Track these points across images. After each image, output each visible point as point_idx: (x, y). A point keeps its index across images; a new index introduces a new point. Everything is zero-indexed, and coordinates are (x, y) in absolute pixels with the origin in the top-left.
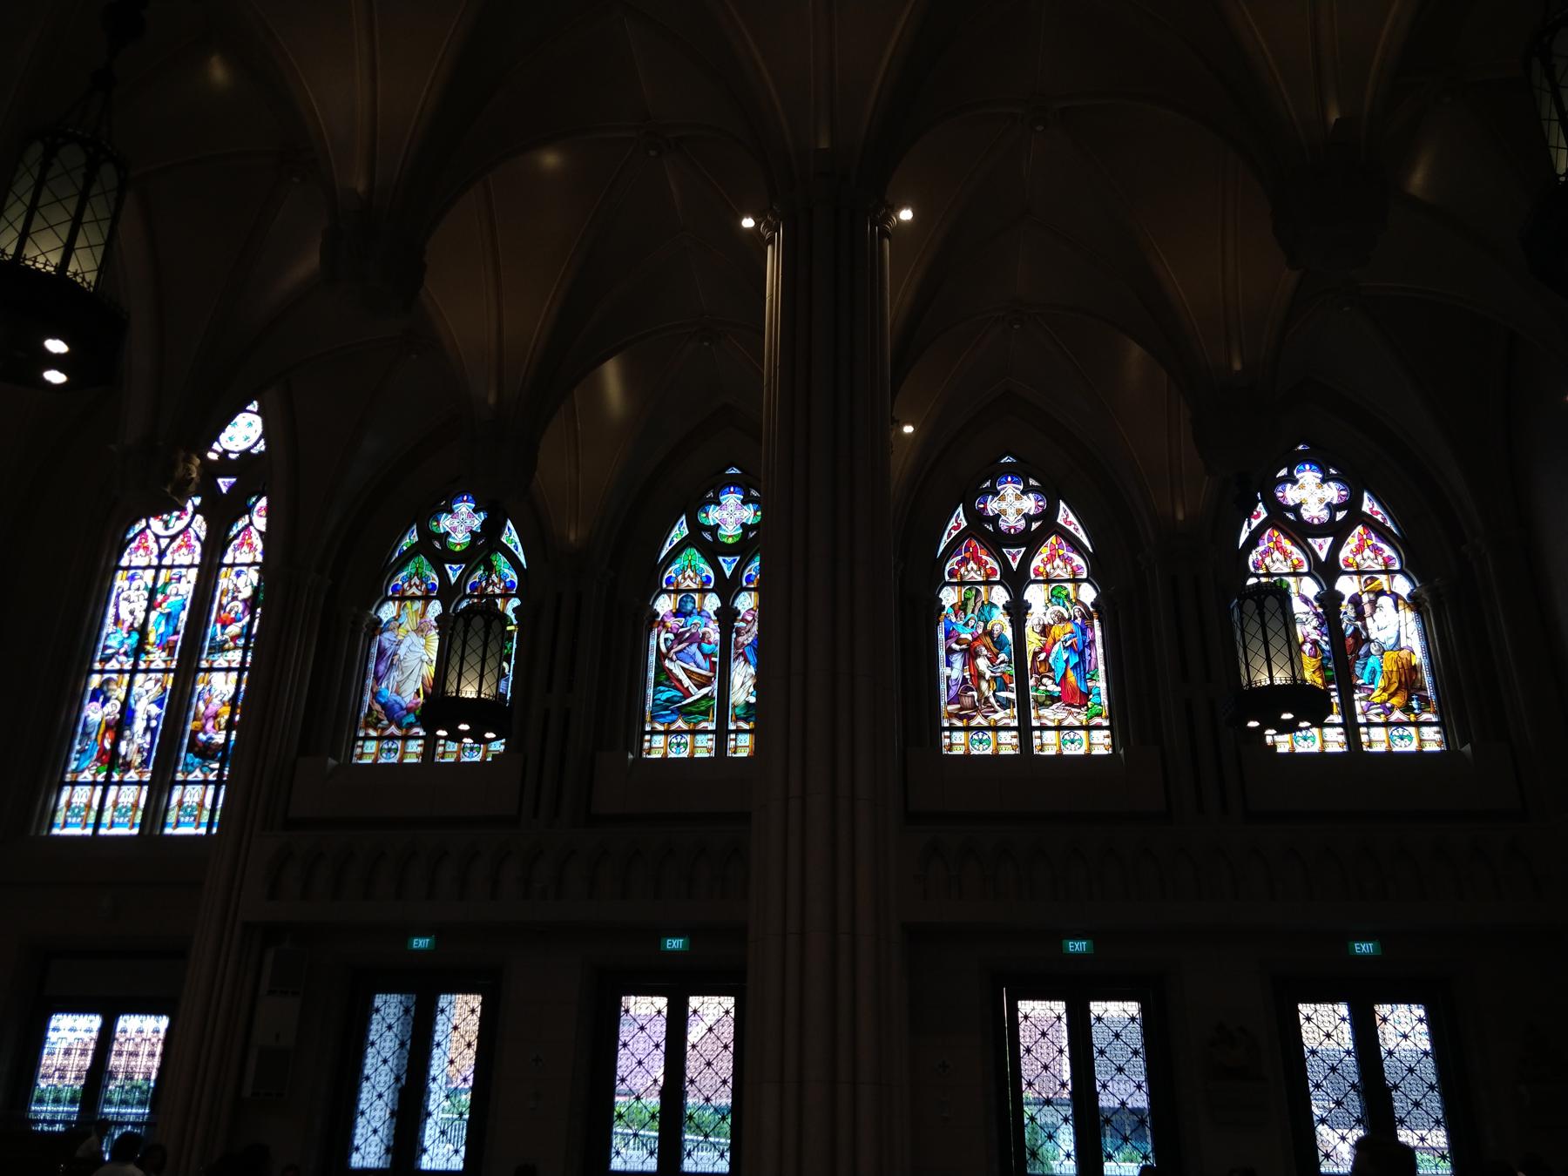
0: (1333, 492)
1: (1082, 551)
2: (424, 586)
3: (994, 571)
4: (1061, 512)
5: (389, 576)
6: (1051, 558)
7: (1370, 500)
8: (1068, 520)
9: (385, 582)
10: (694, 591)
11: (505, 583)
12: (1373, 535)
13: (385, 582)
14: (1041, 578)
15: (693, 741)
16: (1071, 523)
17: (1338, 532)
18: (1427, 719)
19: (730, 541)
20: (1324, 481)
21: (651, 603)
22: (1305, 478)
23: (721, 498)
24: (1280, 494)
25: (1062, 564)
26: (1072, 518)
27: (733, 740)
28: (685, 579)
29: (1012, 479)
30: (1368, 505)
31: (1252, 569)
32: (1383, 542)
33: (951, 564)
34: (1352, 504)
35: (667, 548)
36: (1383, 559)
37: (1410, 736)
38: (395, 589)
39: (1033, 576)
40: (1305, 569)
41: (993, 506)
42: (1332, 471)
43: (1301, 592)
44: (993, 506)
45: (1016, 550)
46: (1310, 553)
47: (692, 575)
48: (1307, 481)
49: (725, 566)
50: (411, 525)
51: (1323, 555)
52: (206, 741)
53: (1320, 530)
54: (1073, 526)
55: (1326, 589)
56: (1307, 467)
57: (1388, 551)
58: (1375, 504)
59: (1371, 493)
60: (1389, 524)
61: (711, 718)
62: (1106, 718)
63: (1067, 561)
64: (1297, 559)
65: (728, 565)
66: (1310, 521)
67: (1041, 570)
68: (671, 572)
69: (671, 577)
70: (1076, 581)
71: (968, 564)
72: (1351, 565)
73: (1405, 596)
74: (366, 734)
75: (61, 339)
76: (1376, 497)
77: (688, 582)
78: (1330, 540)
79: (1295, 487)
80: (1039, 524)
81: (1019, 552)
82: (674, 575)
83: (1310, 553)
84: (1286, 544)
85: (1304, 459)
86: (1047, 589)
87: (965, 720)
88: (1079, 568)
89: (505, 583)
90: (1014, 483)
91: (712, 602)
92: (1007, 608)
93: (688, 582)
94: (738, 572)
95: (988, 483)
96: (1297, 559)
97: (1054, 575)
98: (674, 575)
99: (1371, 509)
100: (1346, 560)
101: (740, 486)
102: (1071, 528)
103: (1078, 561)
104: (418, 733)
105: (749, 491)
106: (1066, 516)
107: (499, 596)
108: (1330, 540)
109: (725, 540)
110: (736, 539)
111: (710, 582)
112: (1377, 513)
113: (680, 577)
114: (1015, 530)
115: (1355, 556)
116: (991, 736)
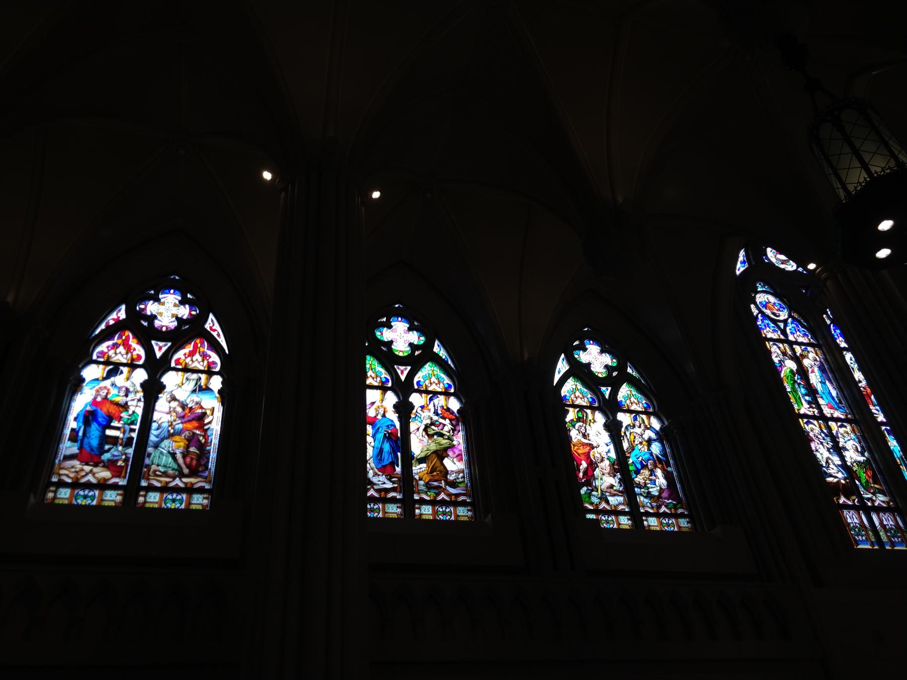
0: (415, 338)
2: (129, 355)
3: (139, 357)
4: (209, 321)
5: (171, 353)
6: (192, 354)
7: (438, 346)
8: (214, 328)
9: (170, 354)
10: (124, 365)
11: (381, 378)
12: (206, 343)
13: (170, 354)
14: (180, 367)
15: (101, 495)
16: (215, 330)
18: (622, 509)
19: (401, 354)
20: (410, 329)
21: (158, 377)
22: (397, 326)
23: (161, 296)
24: (576, 356)
25: (200, 359)
26: (217, 326)
27: (52, 491)
28: (431, 384)
29: (174, 292)
30: (438, 349)
31: (416, 387)
32: (212, 351)
33: (103, 347)
34: (621, 368)
36: (208, 362)
37: (94, 496)
38: (178, 362)
39: (173, 364)
41: (151, 308)
42: (416, 323)
43: (208, 385)
44: (151, 308)
45: (404, 367)
46: (150, 351)
47: (373, 375)
48: (167, 301)
49: (156, 348)
50: (119, 304)
52: (885, 525)
53: (403, 361)
54: (216, 333)
55: (401, 399)
56: (400, 319)
57: (447, 381)
58: (442, 349)
59: (440, 341)
60: (450, 362)
61: (123, 474)
62: (400, 492)
63: (204, 356)
64: (591, 397)
66: (159, 329)
67: (181, 361)
68: (419, 378)
69: (420, 381)
70: (210, 373)
71: (117, 348)
72: (181, 364)
73: (455, 411)
74: (149, 484)
75: (264, 178)
76: (444, 345)
77: (119, 357)
79: (585, 353)
80: (419, 352)
81: (406, 369)
82: (422, 380)
83: (150, 351)
84: (133, 343)
85: (400, 314)
86: (574, 411)
87: (383, 493)
88: (214, 363)
89: (381, 378)
90: (174, 294)
91: (141, 375)
92: (396, 407)
93: (119, 357)
94: (167, 356)
95: (385, 319)
96: (447, 383)
97: (192, 366)
98: (422, 380)
99: (211, 328)
100: (418, 383)
101: (179, 290)
102: (215, 334)
103: (214, 357)
105: (414, 322)
106: (212, 324)
107: (124, 365)
109: (397, 353)
110: (406, 354)
111: (388, 382)
112: (215, 330)
113: (427, 382)
114: (167, 328)
115: (186, 358)
116: (674, 521)
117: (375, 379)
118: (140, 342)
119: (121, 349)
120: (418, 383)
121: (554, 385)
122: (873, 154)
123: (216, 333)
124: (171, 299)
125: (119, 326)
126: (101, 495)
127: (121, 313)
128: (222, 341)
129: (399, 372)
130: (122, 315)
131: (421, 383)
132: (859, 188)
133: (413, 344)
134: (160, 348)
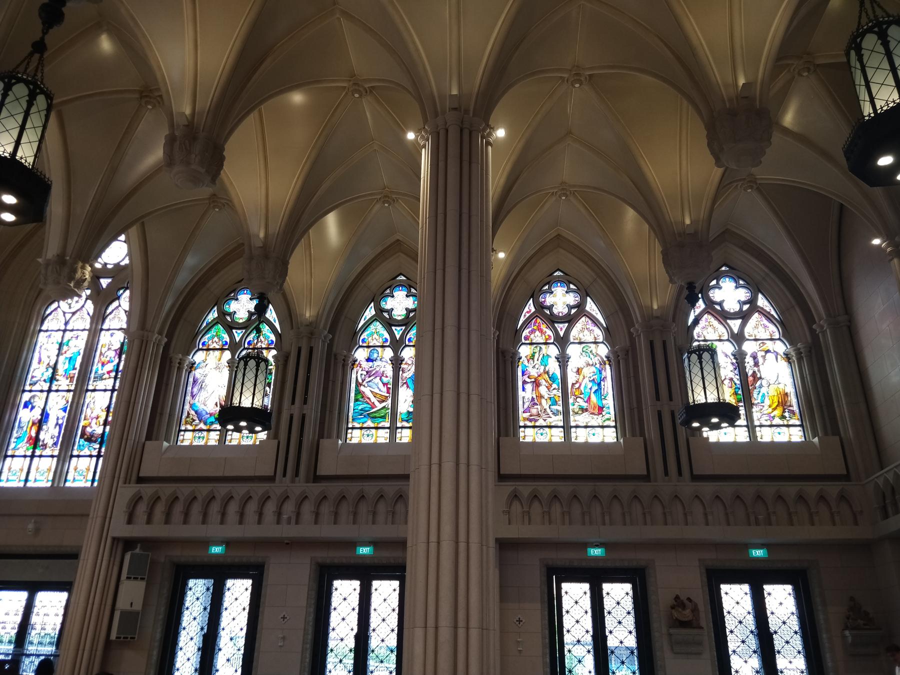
1: (600, 326)
15: (208, 436)
17: (744, 316)
21: (353, 354)
26: (594, 307)
28: (213, 343)
30: (762, 302)
34: (752, 302)
35: (362, 322)
40: (726, 337)
46: (392, 334)
51: (736, 331)
55: (737, 349)
65: (398, 331)
69: (365, 338)
75: (12, 195)
77: (215, 345)
78: (566, 325)
83: (392, 334)
84: (543, 327)
90: (561, 287)
98: (366, 338)
100: (363, 340)
104: (216, 428)
106: (591, 306)
108: (566, 325)
117: (218, 344)
118: (548, 327)
119: (537, 333)
120: (363, 340)
121: (689, 325)
122: (879, 67)
123: (527, 314)
124: (727, 284)
125: (215, 322)
126: (208, 436)
127: (213, 315)
128: (600, 317)
129: (559, 329)
130: (216, 315)
131: (412, 340)
132: (885, 108)
133: (408, 308)
134: (238, 335)
